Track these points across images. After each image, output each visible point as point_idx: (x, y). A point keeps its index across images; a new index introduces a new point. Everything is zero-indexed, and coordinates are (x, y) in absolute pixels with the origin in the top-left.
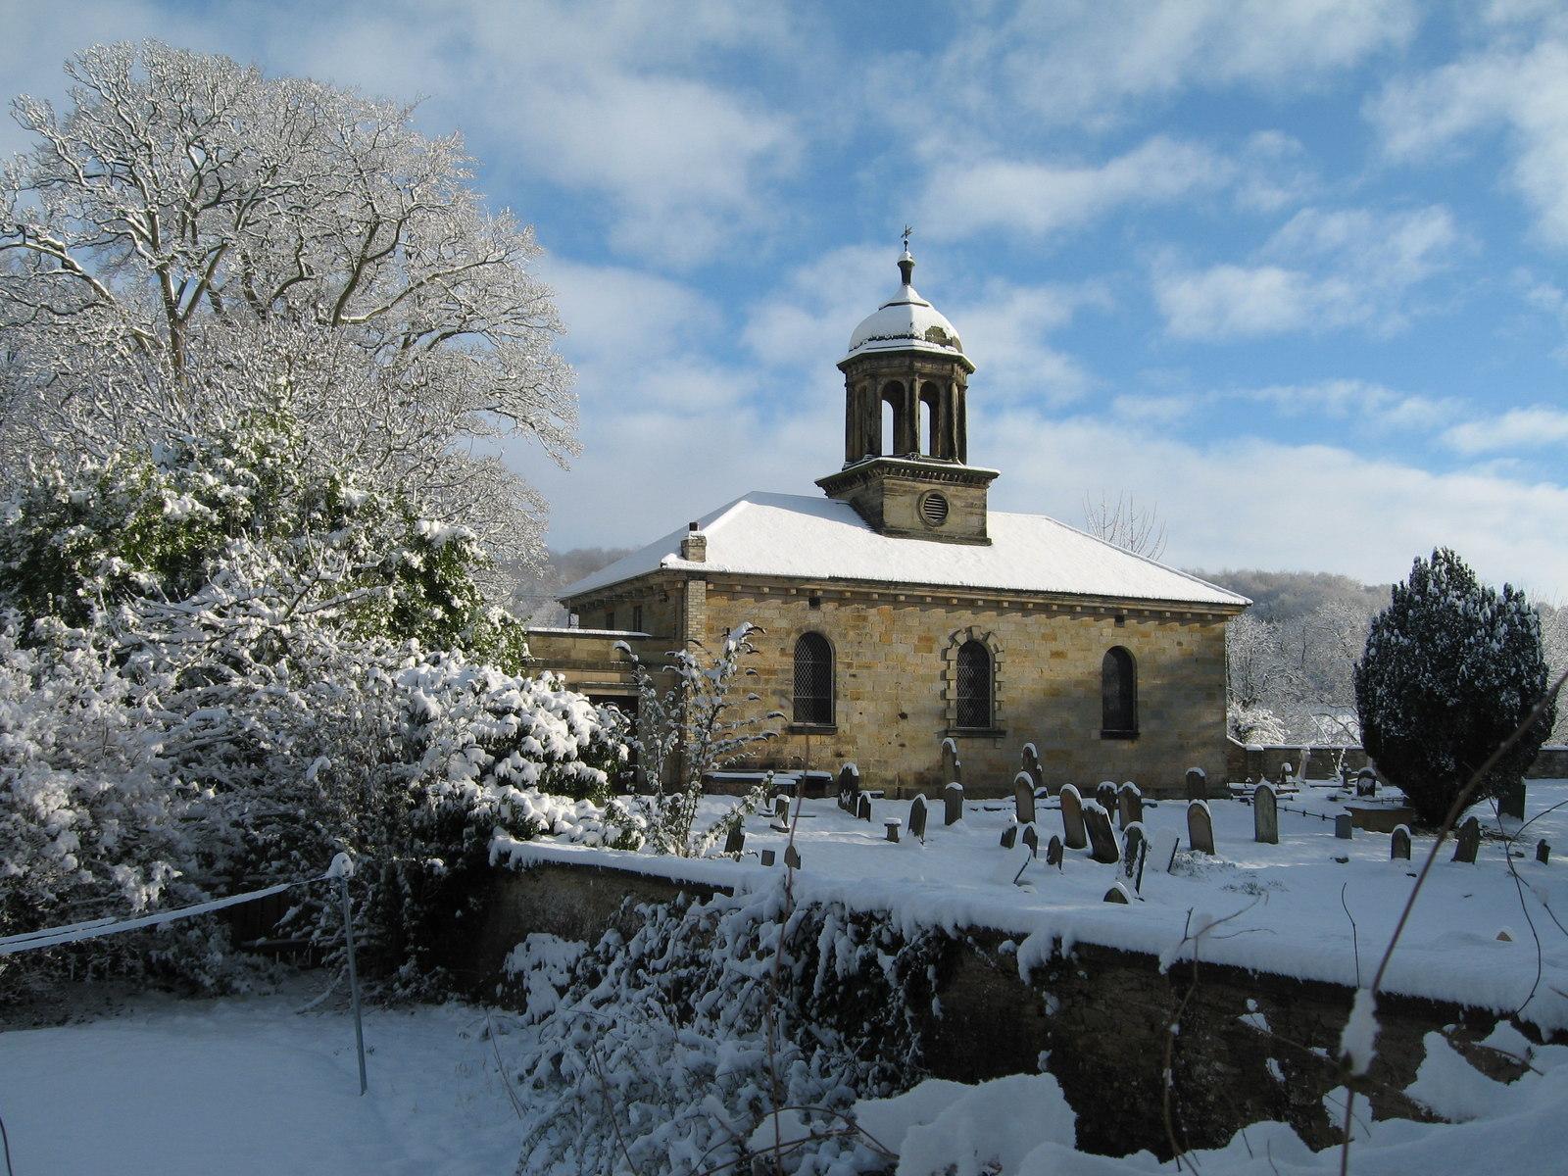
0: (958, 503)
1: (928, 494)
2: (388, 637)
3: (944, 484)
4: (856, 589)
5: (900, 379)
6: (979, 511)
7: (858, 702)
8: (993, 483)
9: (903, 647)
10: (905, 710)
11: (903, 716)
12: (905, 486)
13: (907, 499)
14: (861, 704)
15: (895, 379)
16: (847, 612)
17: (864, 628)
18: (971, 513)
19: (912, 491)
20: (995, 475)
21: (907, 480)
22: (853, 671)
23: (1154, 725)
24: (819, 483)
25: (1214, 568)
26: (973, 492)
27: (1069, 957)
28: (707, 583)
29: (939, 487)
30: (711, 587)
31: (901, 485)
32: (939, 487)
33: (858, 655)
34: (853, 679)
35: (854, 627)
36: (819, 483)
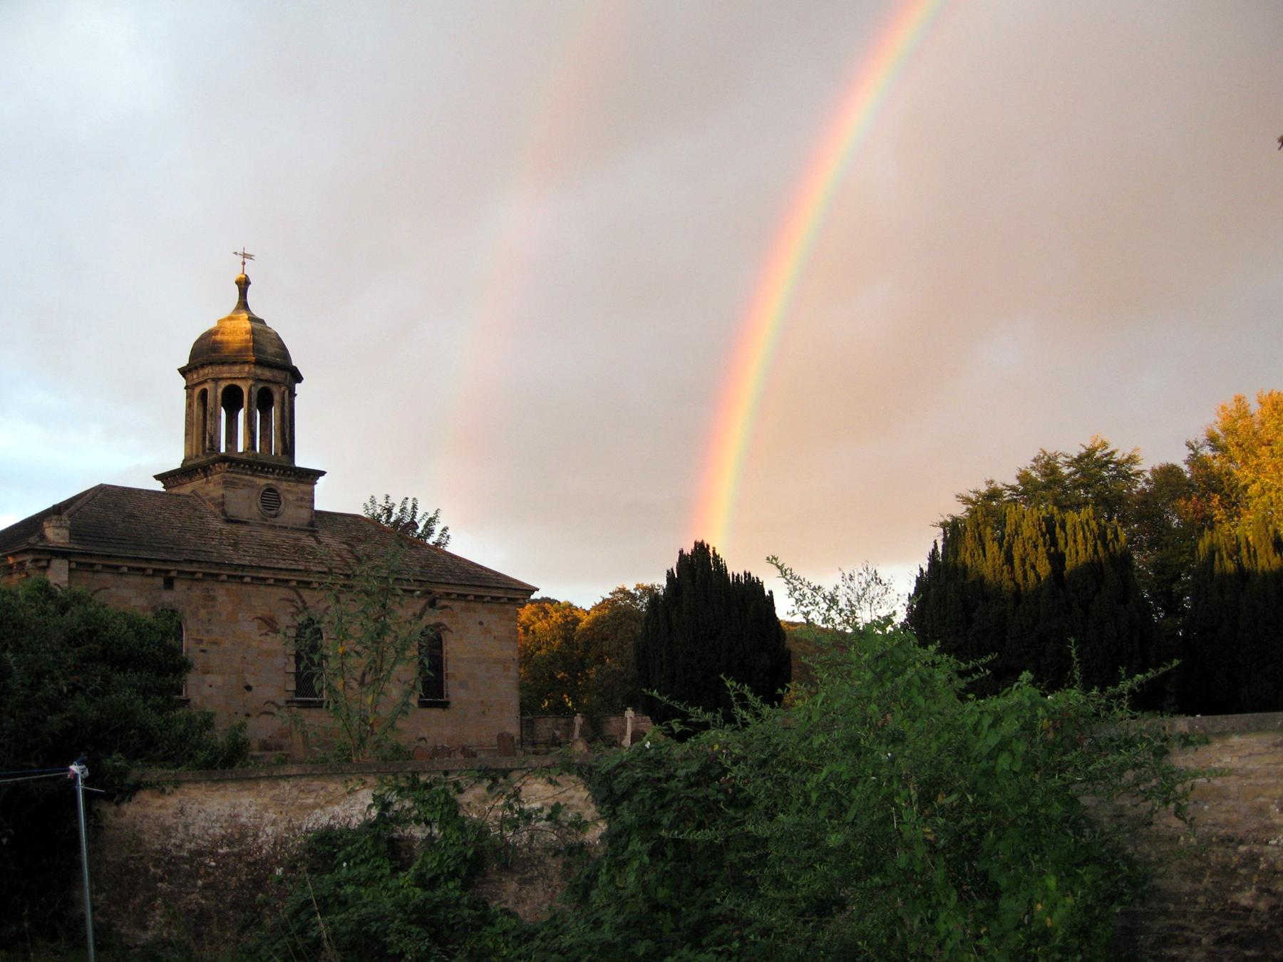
0: (290, 497)
1: (264, 488)
2: (647, 788)
3: (279, 480)
4: (207, 571)
5: (238, 383)
6: (308, 504)
7: (208, 676)
8: (321, 480)
9: (249, 627)
10: (251, 683)
11: (249, 688)
12: (243, 480)
13: (244, 492)
14: (210, 678)
15: (235, 382)
16: (197, 591)
17: (213, 606)
18: (301, 507)
19: (251, 486)
20: (322, 473)
21: (246, 474)
22: (203, 646)
23: (462, 693)
24: (158, 477)
25: (717, 552)
26: (303, 487)
27: (69, 770)
28: (70, 562)
29: (274, 482)
30: (73, 565)
31: (240, 479)
32: (274, 482)
33: (208, 632)
34: (202, 654)
35: (204, 607)
36: (158, 477)
